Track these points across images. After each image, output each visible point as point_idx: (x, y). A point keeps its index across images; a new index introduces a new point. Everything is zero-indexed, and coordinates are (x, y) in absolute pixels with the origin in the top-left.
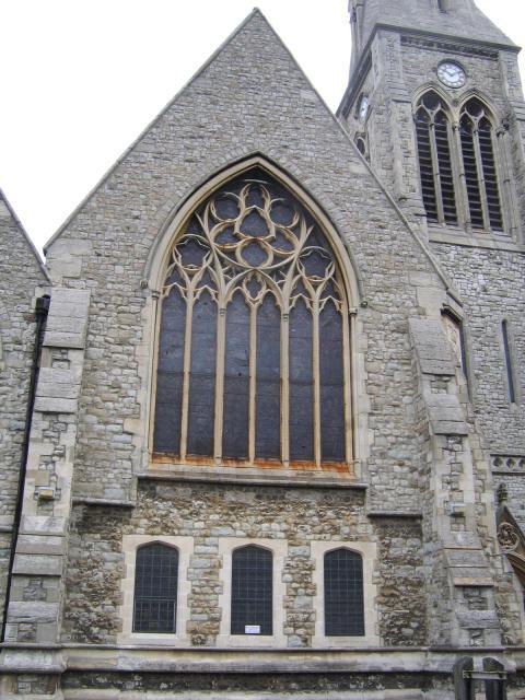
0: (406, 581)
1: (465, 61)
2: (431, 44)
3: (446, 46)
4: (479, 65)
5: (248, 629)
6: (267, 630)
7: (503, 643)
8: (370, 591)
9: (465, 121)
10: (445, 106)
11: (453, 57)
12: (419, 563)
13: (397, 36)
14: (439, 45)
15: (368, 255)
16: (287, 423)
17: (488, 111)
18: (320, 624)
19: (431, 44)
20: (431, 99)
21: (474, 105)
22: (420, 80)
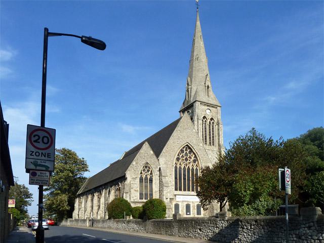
21: (212, 119)
22: (203, 113)
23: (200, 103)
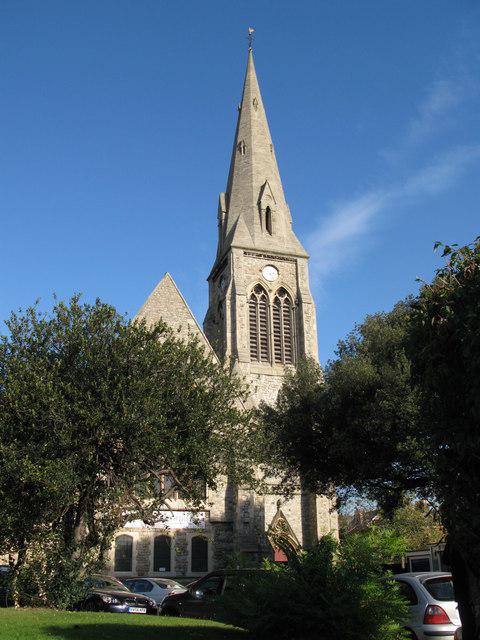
0: (225, 549)
1: (276, 263)
2: (260, 255)
3: (268, 257)
4: (288, 266)
5: (161, 569)
6: (168, 569)
7: (296, 261)
8: (211, 553)
9: (276, 299)
10: (265, 292)
11: (272, 263)
12: (232, 541)
13: (242, 251)
14: (265, 256)
15: (69, 514)
16: (78, 621)
17: (289, 295)
18: (189, 566)
19: (260, 255)
20: (259, 288)
21: (282, 291)
23: (242, 251)
